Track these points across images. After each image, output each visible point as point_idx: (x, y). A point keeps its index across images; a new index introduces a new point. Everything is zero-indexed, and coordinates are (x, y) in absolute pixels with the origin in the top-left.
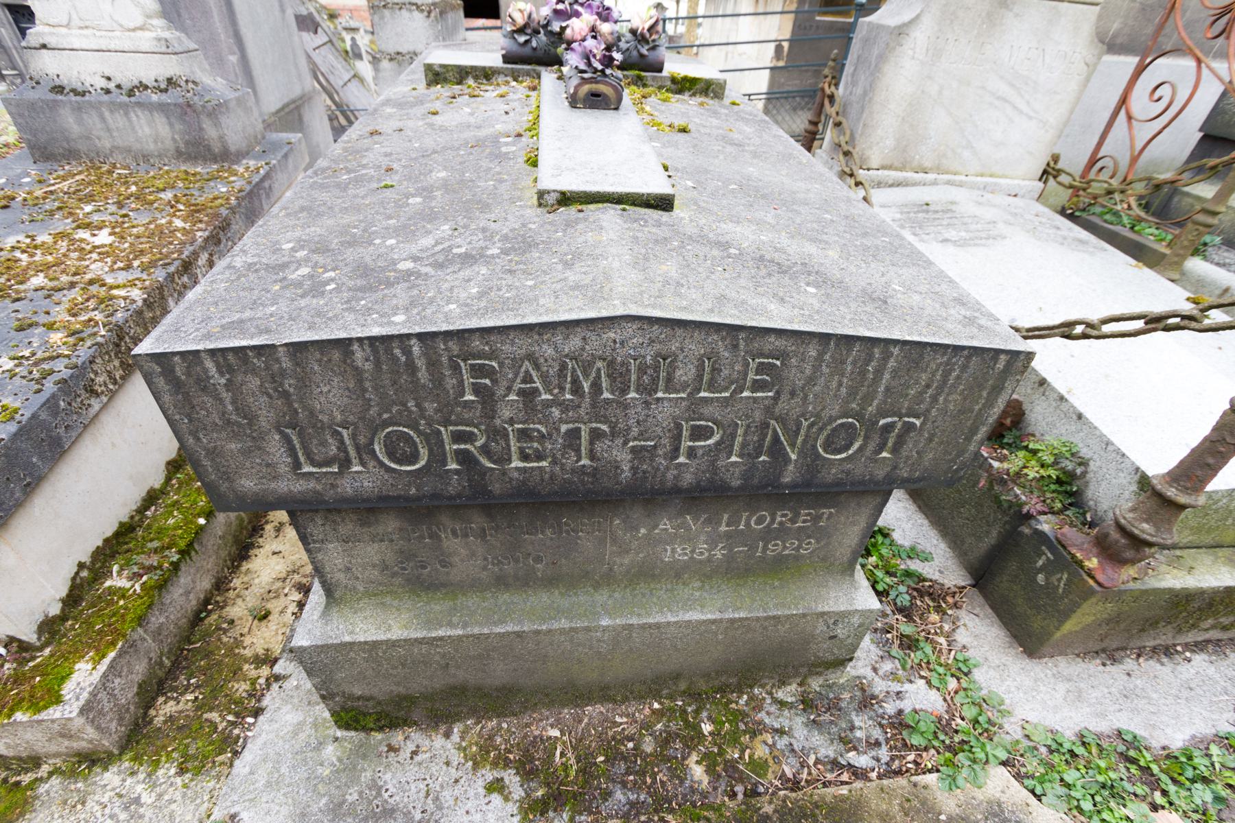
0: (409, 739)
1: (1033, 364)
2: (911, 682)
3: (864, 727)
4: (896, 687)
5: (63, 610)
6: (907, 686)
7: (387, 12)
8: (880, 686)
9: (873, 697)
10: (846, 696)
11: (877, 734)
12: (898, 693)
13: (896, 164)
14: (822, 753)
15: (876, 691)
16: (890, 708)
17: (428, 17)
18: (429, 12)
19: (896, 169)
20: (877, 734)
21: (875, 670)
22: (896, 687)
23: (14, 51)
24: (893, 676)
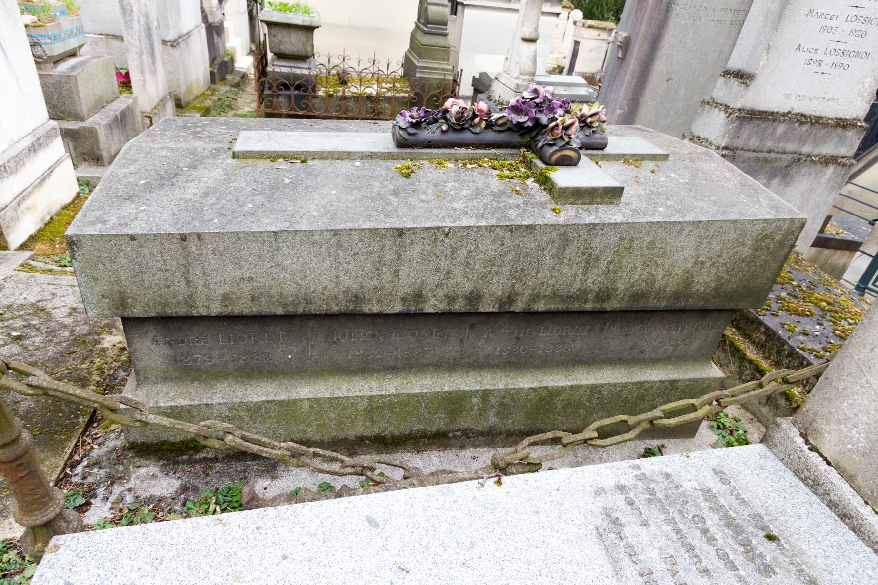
0: (184, 315)
1: (236, 65)
2: (111, 509)
3: (99, 474)
4: (112, 498)
5: (239, 72)
6: (109, 505)
7: (707, 107)
8: (117, 489)
9: (112, 484)
10: (121, 468)
11: (90, 479)
12: (108, 499)
13: (860, 480)
14: (96, 451)
15: (115, 486)
16: (101, 491)
17: (728, 117)
18: (730, 114)
19: (858, 490)
20: (90, 479)
21: (130, 490)
22: (112, 498)
23: (293, 70)
24: (121, 499)
